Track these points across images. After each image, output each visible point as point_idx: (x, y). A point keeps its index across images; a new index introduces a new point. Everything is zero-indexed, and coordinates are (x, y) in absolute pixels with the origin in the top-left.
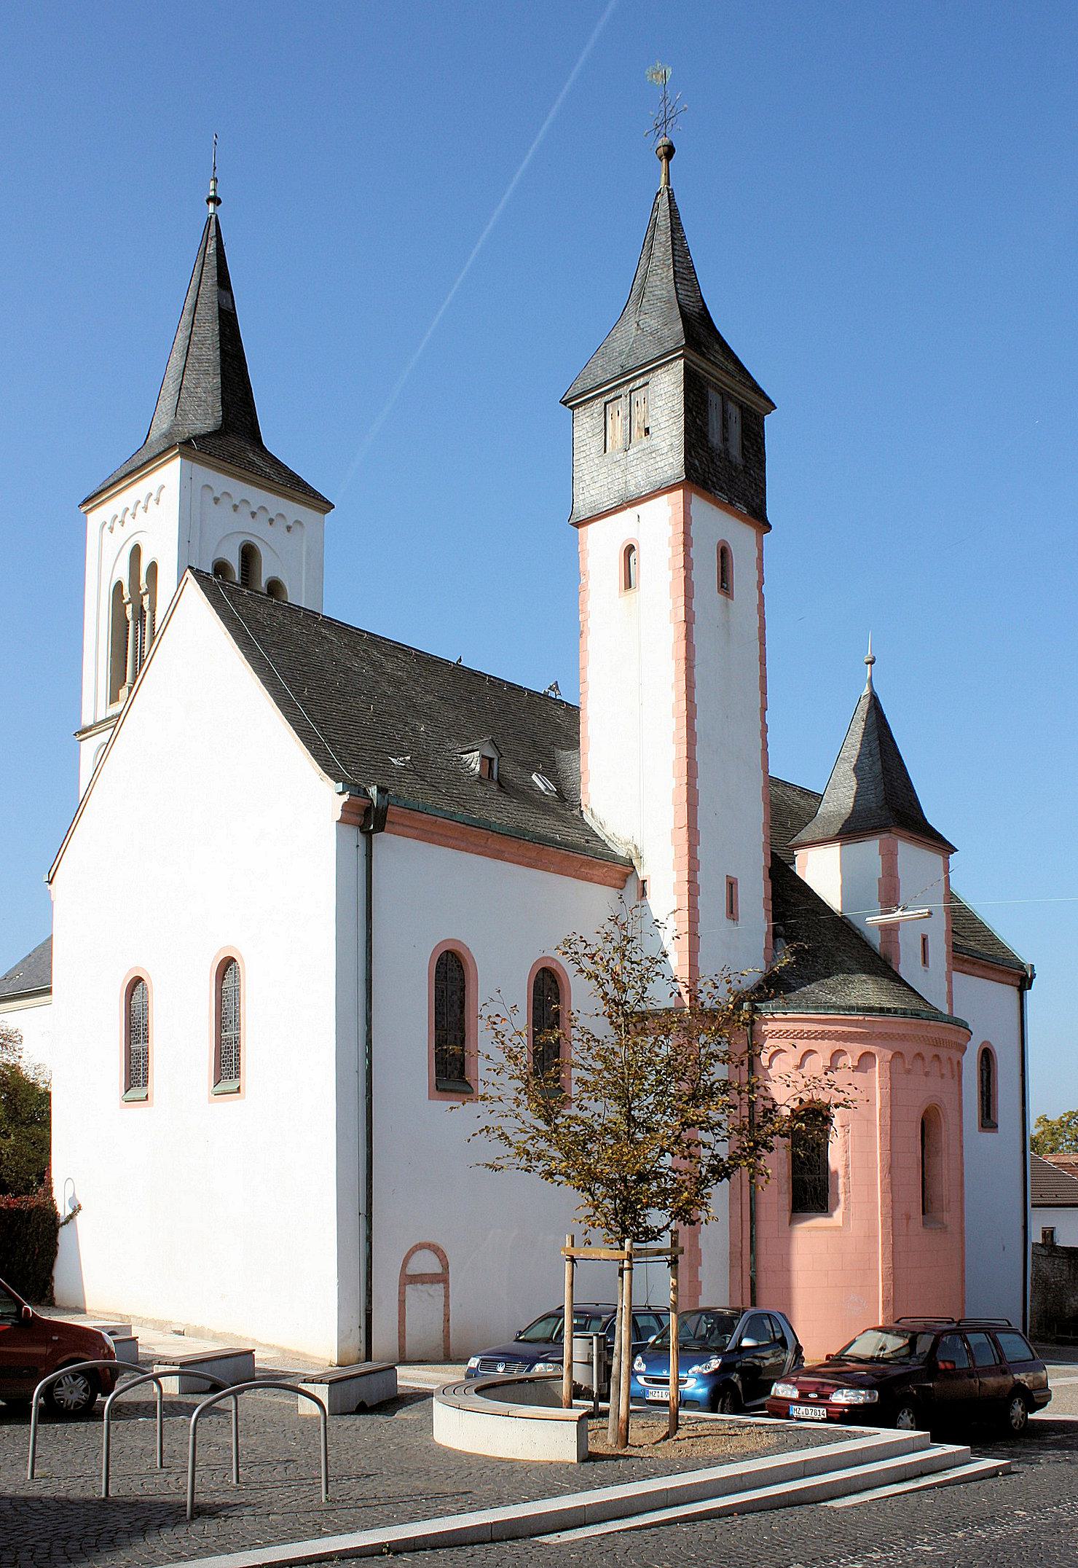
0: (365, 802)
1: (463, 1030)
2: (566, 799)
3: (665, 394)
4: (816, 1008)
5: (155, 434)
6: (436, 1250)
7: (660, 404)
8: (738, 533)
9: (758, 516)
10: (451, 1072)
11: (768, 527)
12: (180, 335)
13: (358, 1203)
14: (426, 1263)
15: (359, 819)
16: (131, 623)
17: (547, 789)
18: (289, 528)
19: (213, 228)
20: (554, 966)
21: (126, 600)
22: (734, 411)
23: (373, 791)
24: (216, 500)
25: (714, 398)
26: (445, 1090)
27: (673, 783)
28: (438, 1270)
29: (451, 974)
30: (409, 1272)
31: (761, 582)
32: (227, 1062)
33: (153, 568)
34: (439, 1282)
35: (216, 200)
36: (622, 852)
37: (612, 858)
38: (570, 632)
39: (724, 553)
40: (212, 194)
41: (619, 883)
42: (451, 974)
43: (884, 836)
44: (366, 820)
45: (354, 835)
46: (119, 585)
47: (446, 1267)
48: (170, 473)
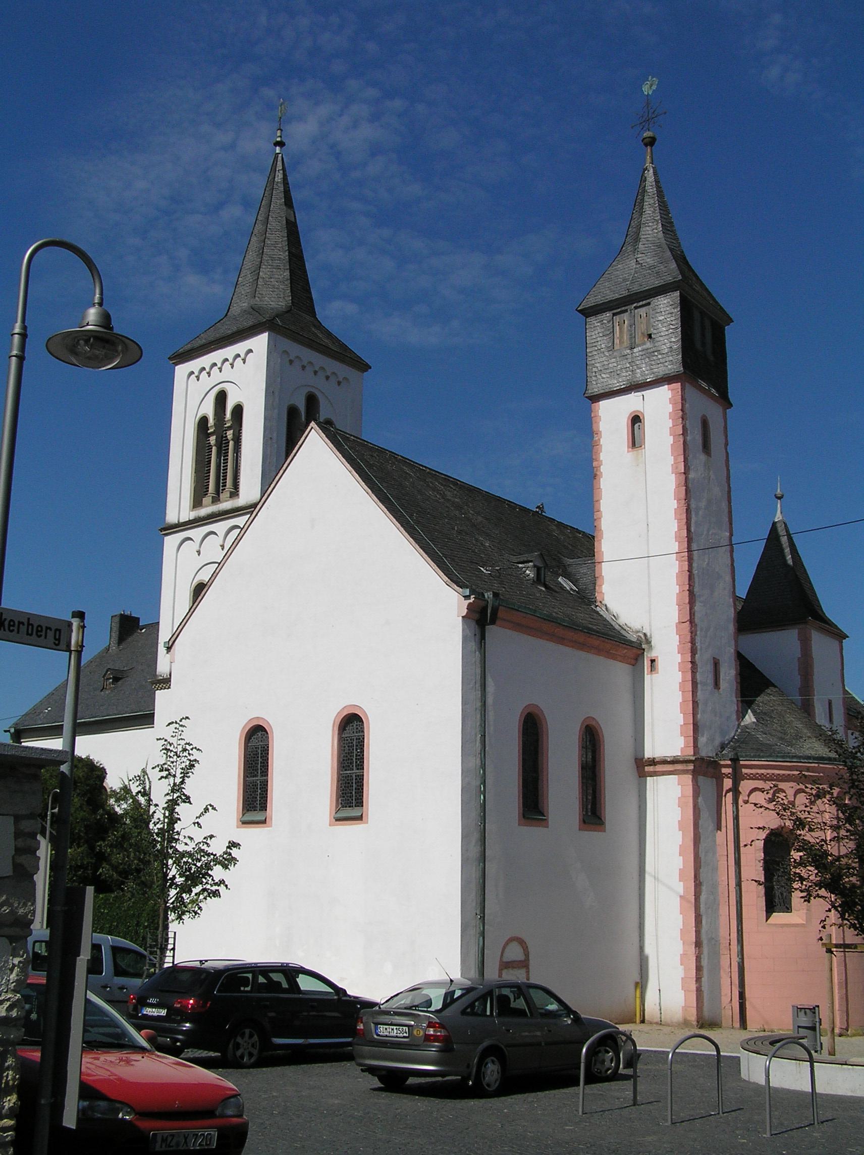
0: (483, 604)
1: (595, 781)
2: (586, 597)
3: (665, 314)
4: (783, 757)
5: (235, 310)
6: (522, 942)
7: (660, 318)
8: (713, 411)
9: (724, 399)
10: (533, 806)
11: (730, 405)
12: (254, 239)
13: (475, 851)
14: (515, 953)
15: (477, 616)
16: (214, 449)
17: (571, 589)
18: (339, 383)
19: (279, 163)
20: (594, 723)
21: (211, 430)
22: (707, 323)
23: (488, 595)
24: (291, 362)
25: (696, 314)
26: (528, 818)
27: (676, 589)
28: (521, 957)
29: (532, 730)
30: (505, 960)
31: (726, 444)
32: (350, 794)
33: (238, 410)
34: (523, 967)
35: (281, 144)
36: (633, 638)
37: (627, 643)
38: (584, 473)
39: (705, 424)
40: (279, 139)
41: (633, 662)
42: (532, 730)
43: (801, 626)
44: (480, 619)
45: (473, 624)
46: (203, 421)
47: (527, 955)
48: (260, 343)
